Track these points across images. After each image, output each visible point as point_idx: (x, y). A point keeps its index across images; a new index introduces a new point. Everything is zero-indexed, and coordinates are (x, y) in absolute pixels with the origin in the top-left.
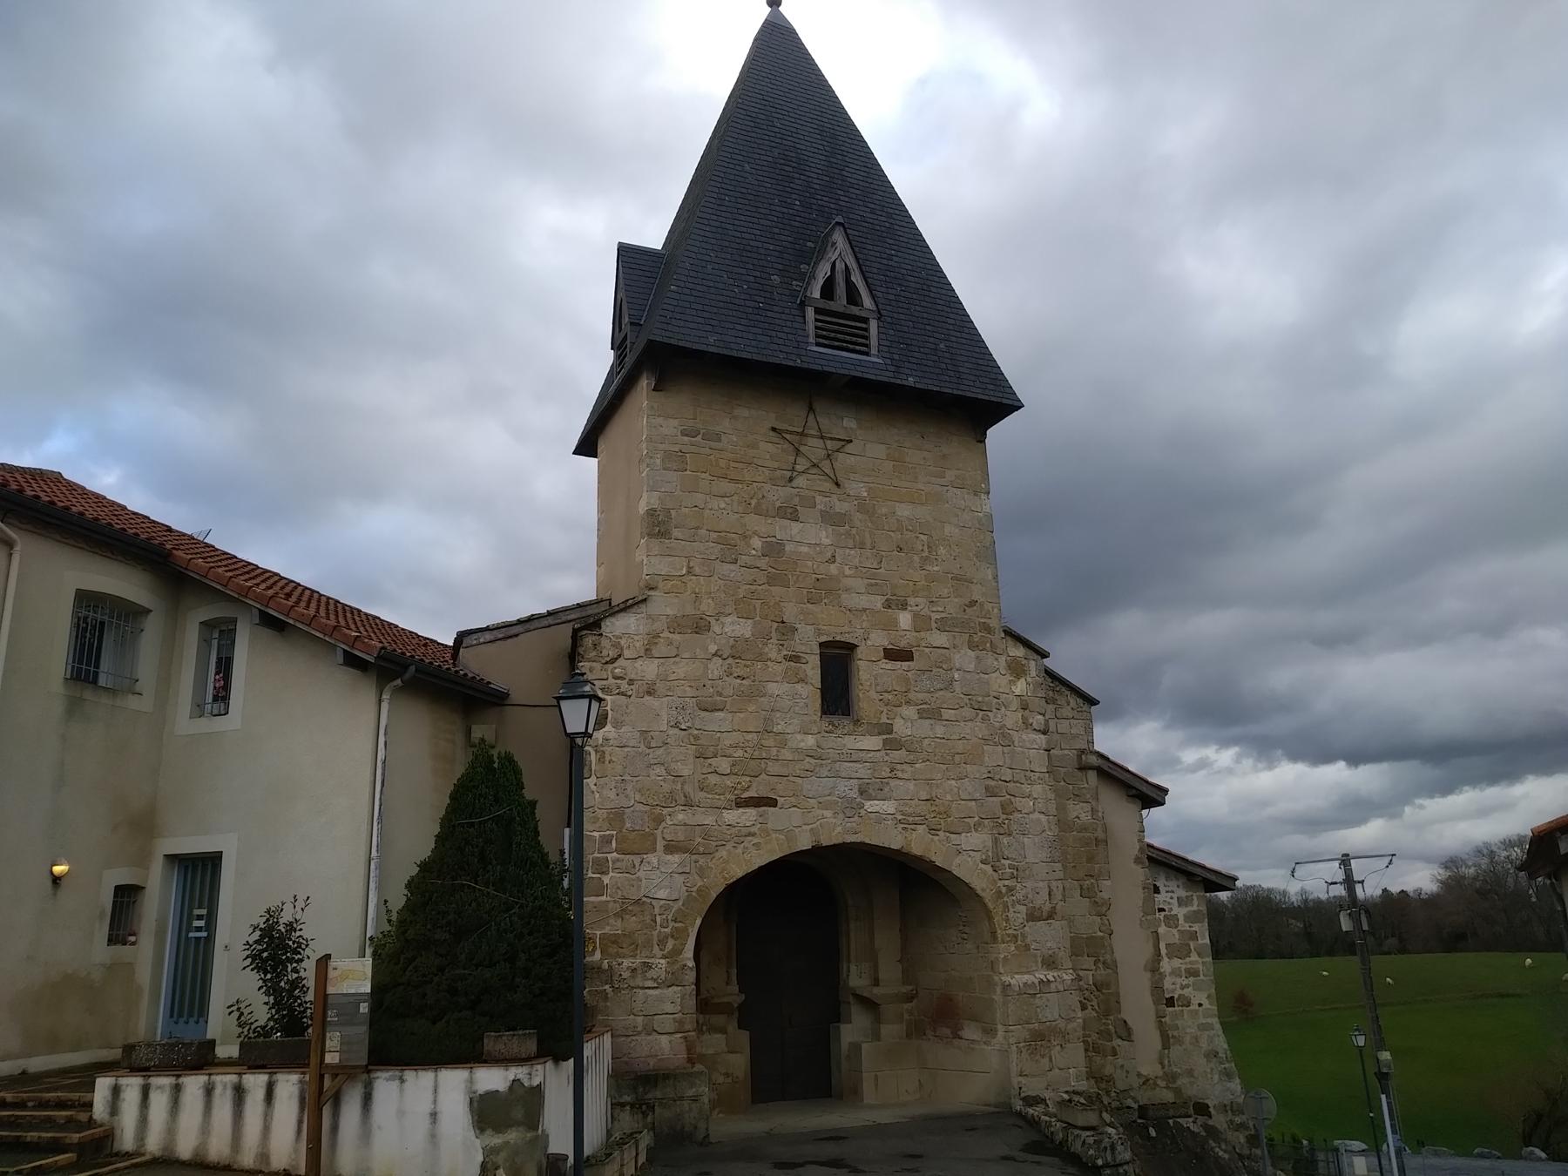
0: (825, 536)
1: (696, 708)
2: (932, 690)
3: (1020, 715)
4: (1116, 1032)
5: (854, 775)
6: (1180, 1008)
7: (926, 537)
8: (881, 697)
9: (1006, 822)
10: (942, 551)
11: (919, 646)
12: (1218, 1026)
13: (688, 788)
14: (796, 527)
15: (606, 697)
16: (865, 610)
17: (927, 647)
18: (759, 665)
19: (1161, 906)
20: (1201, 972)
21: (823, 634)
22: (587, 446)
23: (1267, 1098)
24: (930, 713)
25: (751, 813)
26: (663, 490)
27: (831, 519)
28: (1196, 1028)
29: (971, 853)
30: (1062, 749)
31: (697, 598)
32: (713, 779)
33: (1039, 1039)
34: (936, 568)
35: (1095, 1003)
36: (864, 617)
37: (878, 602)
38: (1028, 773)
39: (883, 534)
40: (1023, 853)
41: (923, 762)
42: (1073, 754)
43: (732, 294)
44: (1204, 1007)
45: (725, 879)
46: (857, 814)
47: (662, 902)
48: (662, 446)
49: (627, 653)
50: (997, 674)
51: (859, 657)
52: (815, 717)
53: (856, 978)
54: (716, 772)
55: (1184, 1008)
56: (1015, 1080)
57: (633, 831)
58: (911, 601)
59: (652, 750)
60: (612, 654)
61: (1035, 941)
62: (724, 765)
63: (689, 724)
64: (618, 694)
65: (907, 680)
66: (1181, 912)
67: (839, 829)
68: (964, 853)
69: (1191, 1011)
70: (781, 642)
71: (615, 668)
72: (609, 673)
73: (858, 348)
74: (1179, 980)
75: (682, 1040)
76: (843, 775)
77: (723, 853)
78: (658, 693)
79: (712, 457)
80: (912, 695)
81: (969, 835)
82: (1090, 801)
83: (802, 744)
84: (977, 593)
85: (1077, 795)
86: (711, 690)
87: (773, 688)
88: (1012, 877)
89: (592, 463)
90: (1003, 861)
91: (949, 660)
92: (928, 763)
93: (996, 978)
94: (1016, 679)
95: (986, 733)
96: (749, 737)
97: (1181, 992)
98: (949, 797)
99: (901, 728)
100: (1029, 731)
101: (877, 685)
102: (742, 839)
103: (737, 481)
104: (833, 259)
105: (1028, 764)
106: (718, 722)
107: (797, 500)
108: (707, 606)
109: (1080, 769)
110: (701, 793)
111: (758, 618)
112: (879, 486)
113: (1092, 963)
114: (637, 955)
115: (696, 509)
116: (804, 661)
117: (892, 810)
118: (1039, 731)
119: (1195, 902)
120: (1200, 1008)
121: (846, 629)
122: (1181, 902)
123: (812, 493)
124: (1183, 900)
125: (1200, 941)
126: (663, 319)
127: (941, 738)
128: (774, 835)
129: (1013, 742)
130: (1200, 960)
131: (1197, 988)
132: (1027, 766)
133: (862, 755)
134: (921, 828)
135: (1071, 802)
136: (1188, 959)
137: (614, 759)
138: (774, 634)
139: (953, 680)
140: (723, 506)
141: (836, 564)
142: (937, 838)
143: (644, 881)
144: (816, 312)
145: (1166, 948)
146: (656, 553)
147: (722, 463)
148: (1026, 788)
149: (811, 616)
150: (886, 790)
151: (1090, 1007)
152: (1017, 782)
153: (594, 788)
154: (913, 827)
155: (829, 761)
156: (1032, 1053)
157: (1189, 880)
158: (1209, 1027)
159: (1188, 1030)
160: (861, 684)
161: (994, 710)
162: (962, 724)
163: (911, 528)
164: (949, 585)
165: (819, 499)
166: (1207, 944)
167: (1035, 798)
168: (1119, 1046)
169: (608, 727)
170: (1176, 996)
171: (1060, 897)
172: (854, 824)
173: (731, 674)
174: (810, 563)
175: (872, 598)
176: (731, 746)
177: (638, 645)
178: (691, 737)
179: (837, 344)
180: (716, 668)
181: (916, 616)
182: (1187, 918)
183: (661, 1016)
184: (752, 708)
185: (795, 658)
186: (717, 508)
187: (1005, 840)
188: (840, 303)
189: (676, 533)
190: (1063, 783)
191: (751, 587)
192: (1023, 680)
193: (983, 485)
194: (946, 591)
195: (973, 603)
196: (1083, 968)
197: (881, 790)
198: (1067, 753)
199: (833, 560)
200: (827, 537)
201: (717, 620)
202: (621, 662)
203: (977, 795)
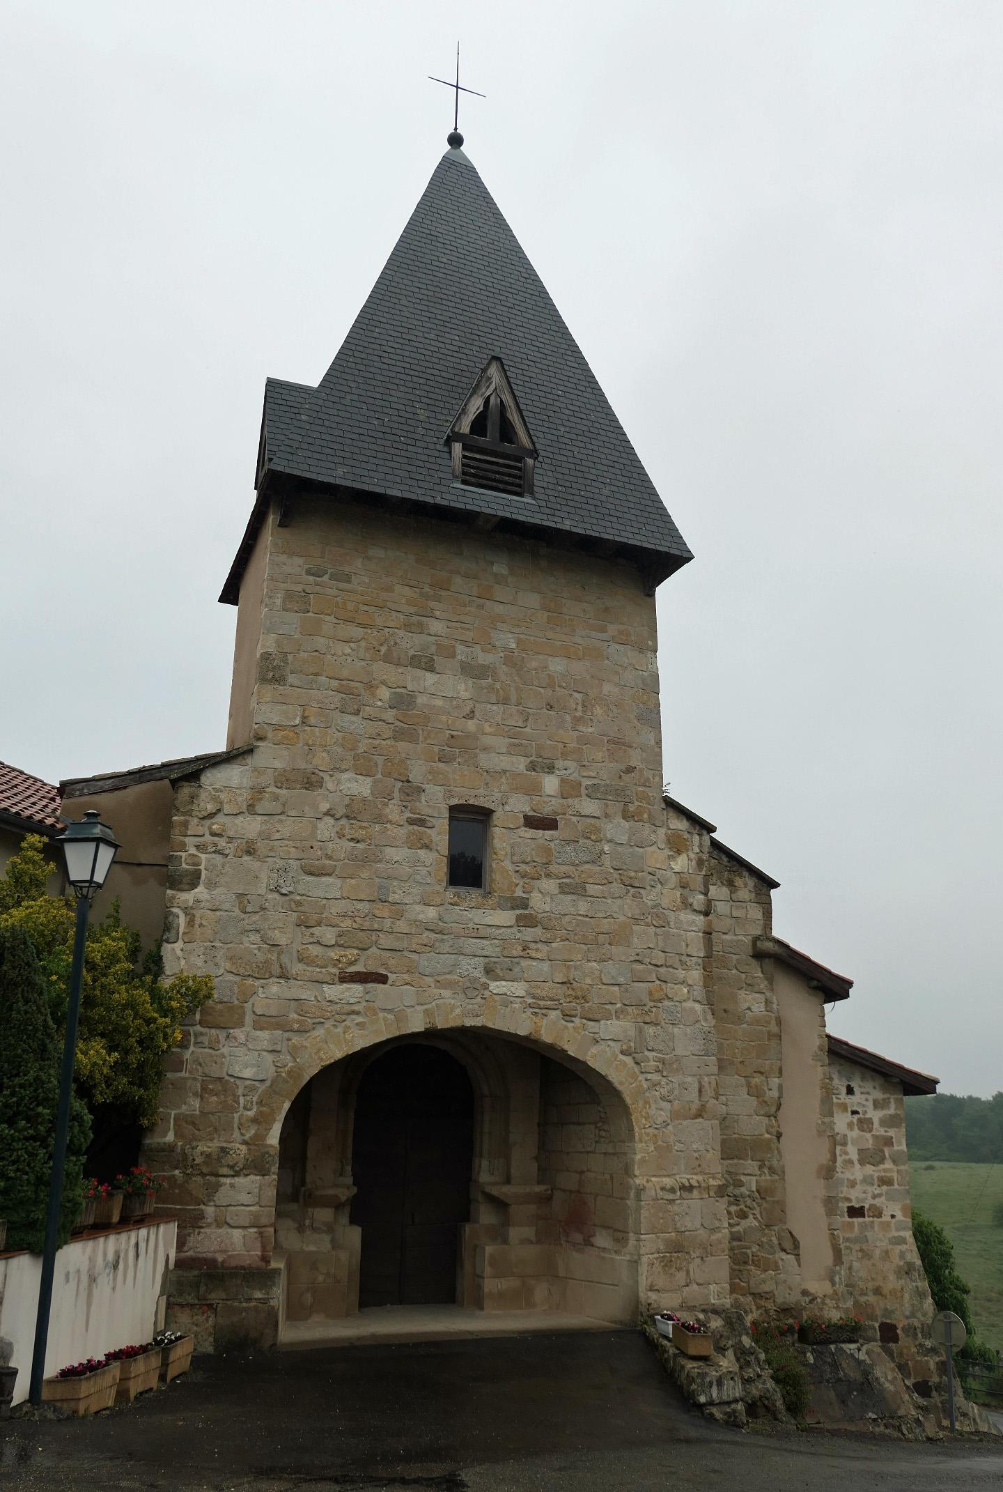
0: (463, 689)
1: (301, 871)
2: (577, 862)
3: (678, 894)
4: (780, 1244)
5: (479, 952)
6: (871, 1219)
7: (581, 695)
8: (517, 869)
9: (654, 1010)
10: (598, 711)
11: (564, 814)
12: (911, 1240)
13: (285, 959)
14: (430, 678)
15: (200, 855)
16: (505, 772)
17: (574, 815)
18: (377, 827)
19: (854, 1109)
20: (896, 1180)
21: (453, 796)
22: (230, 594)
23: (955, 1322)
24: (574, 889)
25: (357, 989)
26: (281, 632)
27: (471, 670)
28: (887, 1241)
29: (610, 1042)
30: (735, 935)
31: (310, 748)
32: (315, 950)
33: (677, 1250)
34: (590, 730)
35: (757, 1212)
36: (503, 780)
37: (521, 764)
38: (684, 958)
39: (531, 689)
40: (671, 1044)
41: (562, 941)
42: (747, 940)
43: (372, 427)
44: (897, 1218)
45: (322, 1059)
46: (480, 996)
47: (248, 1082)
48: (283, 586)
49: (227, 809)
50: (653, 848)
51: (496, 823)
52: (438, 888)
53: (485, 1175)
54: (318, 942)
55: (875, 1219)
56: (643, 1295)
57: (221, 1003)
58: (560, 764)
59: (249, 915)
60: (210, 807)
61: (680, 1142)
62: (329, 935)
63: (291, 889)
64: (214, 852)
65: (548, 851)
66: (876, 1116)
67: (458, 1011)
68: (602, 1042)
69: (882, 1223)
70: (404, 803)
71: (213, 824)
72: (206, 828)
73: (509, 488)
74: (870, 1189)
75: (257, 1235)
76: (468, 952)
77: (319, 1032)
78: (259, 853)
79: (339, 599)
80: (553, 868)
81: (609, 1022)
82: (764, 991)
83: (421, 917)
84: (635, 759)
85: (750, 985)
86: (319, 853)
87: (393, 854)
88: (658, 1071)
89: (232, 610)
90: (647, 1053)
91: (598, 830)
92: (567, 942)
93: (631, 1181)
94: (676, 855)
95: (638, 911)
96: (359, 906)
97: (873, 1202)
98: (588, 981)
99: (538, 903)
100: (688, 911)
101: (513, 855)
102: (344, 1017)
103: (365, 626)
104: (488, 394)
105: (684, 947)
106: (328, 887)
107: (433, 648)
108: (321, 760)
109: (759, 955)
110: (300, 965)
111: (379, 776)
112: (529, 638)
113: (757, 1168)
114: (214, 1139)
115: (316, 653)
116: (430, 825)
117: (522, 993)
118: (700, 912)
119: (893, 1105)
120: (893, 1220)
121: (481, 792)
122: (877, 1104)
123: (453, 643)
124: (879, 1103)
125: (896, 1148)
126: (289, 449)
127: (583, 916)
128: (381, 1015)
129: (669, 923)
130: (895, 1168)
131: (891, 1198)
132: (683, 950)
133: (489, 930)
134: (554, 1015)
135: (743, 992)
136: (882, 1167)
137: (204, 923)
138: (396, 794)
139: (602, 852)
140: (348, 651)
141: (475, 721)
142: (572, 1025)
143: (228, 1058)
144: (464, 449)
145: (859, 1154)
146: (268, 700)
147: (350, 606)
148: (681, 974)
149: (441, 776)
150: (516, 970)
151: (751, 1216)
152: (670, 966)
153: (179, 953)
154: (544, 1011)
155: (452, 936)
156: (666, 1265)
157: (886, 1081)
158: (902, 1241)
159: (878, 1244)
160: (495, 853)
161: (649, 888)
162: (609, 901)
163: (564, 685)
164: (605, 749)
165: (460, 648)
166: (904, 1152)
167: (690, 985)
168: (782, 1260)
169: (200, 889)
170: (867, 1206)
171: (713, 1094)
172: (476, 1006)
173: (344, 836)
174: (444, 718)
175: (514, 759)
176: (338, 915)
177: (240, 799)
178: (292, 903)
179: (485, 482)
180: (326, 828)
181: (563, 781)
182: (884, 1123)
183: (236, 1208)
184: (365, 874)
185: (421, 822)
186: (340, 653)
187: (651, 1030)
188: (490, 438)
189: (292, 679)
190: (734, 971)
191: (374, 741)
192: (684, 856)
193: (650, 642)
194: (600, 755)
195: (630, 770)
196: (746, 1172)
197: (511, 970)
198: (736, 938)
199: (471, 715)
200: (466, 690)
201: (331, 776)
202: (220, 818)
203: (621, 980)
